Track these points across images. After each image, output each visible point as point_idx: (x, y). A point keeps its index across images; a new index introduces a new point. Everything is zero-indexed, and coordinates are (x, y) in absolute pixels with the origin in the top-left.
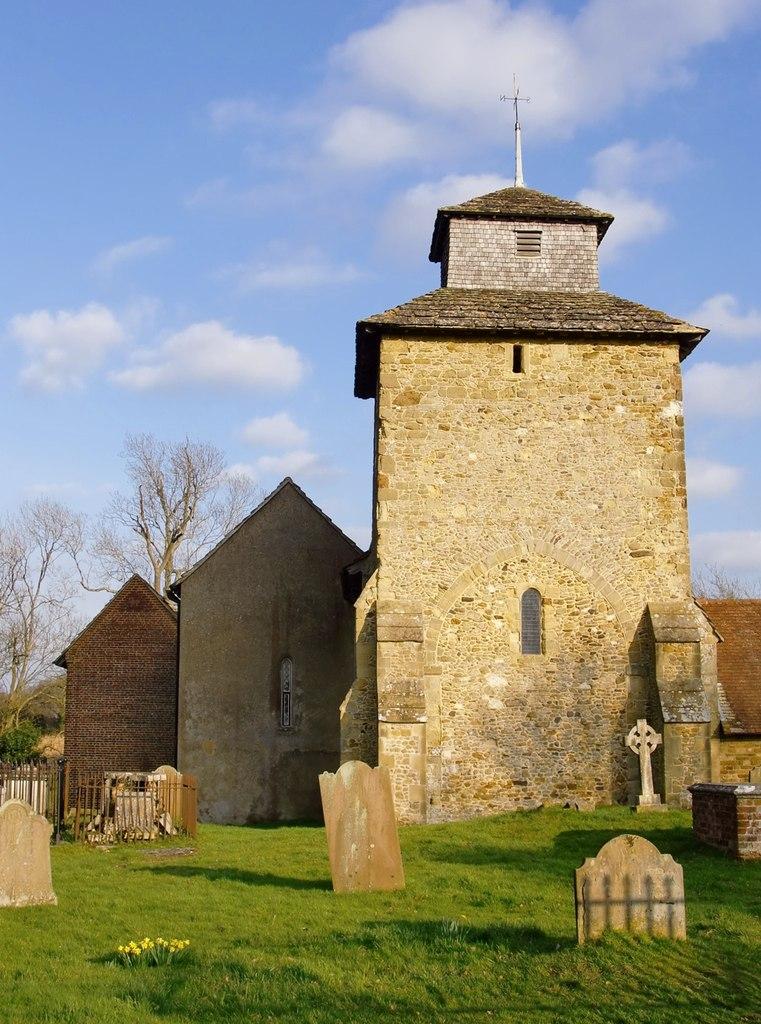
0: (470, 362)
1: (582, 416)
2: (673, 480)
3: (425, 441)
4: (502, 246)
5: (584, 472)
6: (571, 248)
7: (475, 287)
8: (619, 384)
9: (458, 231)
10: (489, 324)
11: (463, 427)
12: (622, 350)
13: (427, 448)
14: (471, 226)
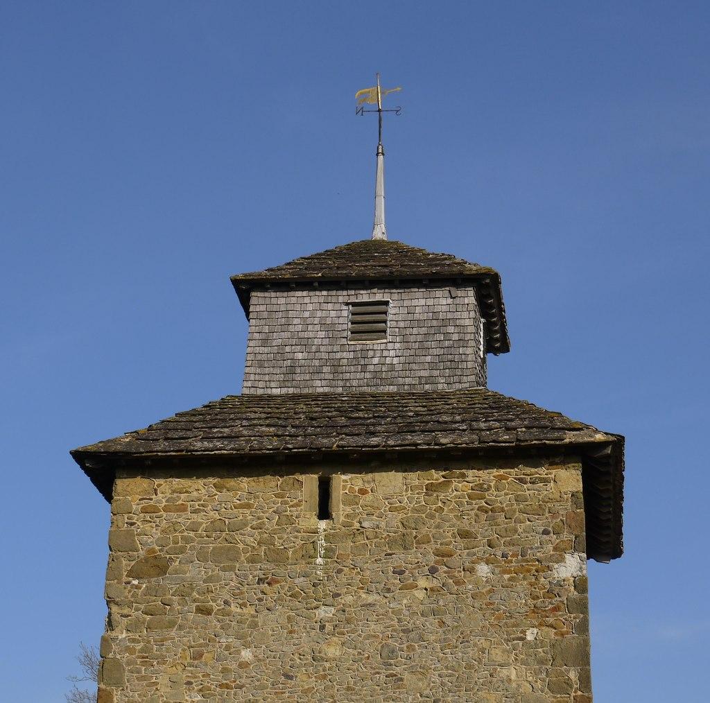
0: (248, 506)
1: (422, 583)
2: (569, 683)
3: (173, 633)
4: (329, 327)
5: (423, 672)
6: (435, 323)
7: (284, 391)
8: (483, 531)
9: (262, 308)
10: (270, 444)
11: (234, 608)
12: (489, 475)
13: (178, 642)
14: (282, 301)
